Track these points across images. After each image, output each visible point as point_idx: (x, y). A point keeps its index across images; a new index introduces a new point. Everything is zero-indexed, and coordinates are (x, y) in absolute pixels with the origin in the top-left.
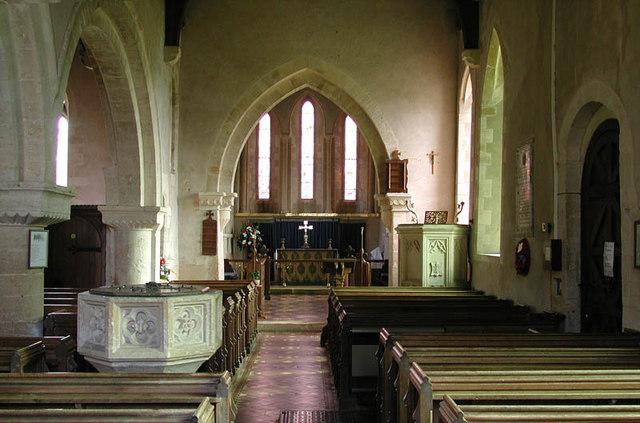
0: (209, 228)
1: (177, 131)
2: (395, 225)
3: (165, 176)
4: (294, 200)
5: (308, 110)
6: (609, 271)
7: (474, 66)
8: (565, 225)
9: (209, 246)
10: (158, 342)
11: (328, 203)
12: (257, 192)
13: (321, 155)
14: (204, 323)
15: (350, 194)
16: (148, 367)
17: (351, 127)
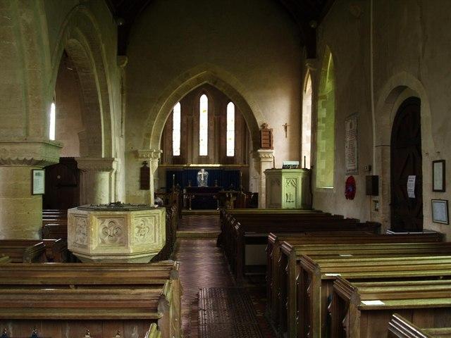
0: (145, 171)
1: (124, 111)
2: (263, 169)
3: (117, 138)
4: (195, 157)
5: (204, 100)
6: (411, 194)
7: (312, 69)
8: (380, 167)
9: (144, 184)
10: (124, 243)
11: (217, 158)
12: (172, 152)
13: (212, 128)
14: (155, 230)
15: (230, 152)
16: (117, 259)
17: (231, 108)
